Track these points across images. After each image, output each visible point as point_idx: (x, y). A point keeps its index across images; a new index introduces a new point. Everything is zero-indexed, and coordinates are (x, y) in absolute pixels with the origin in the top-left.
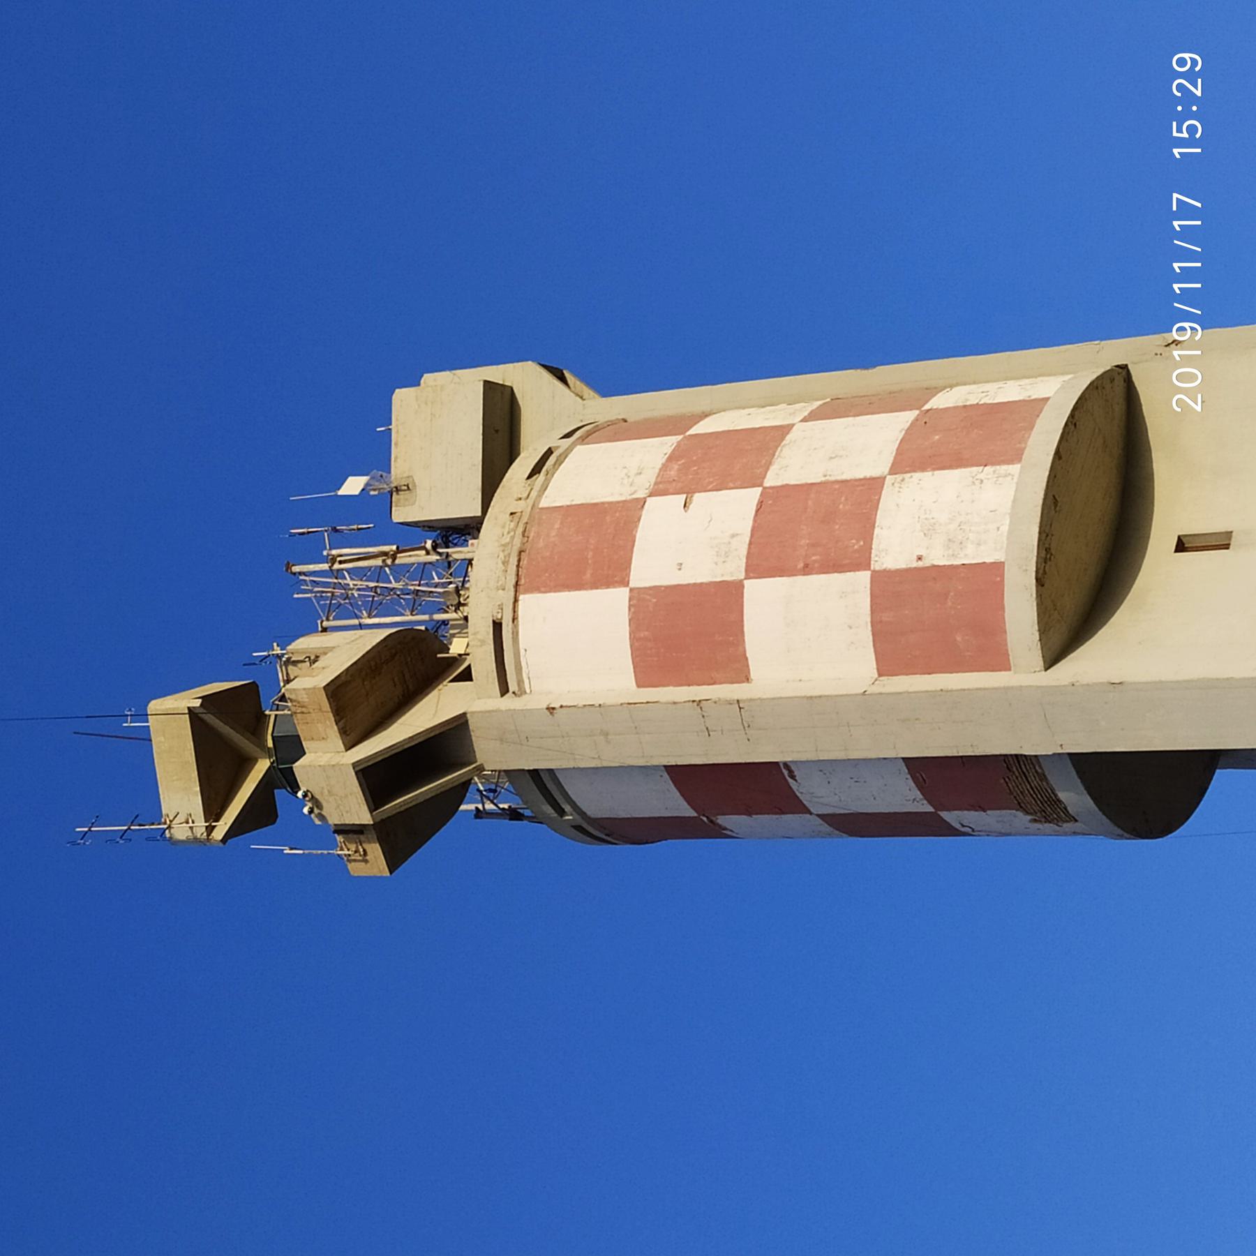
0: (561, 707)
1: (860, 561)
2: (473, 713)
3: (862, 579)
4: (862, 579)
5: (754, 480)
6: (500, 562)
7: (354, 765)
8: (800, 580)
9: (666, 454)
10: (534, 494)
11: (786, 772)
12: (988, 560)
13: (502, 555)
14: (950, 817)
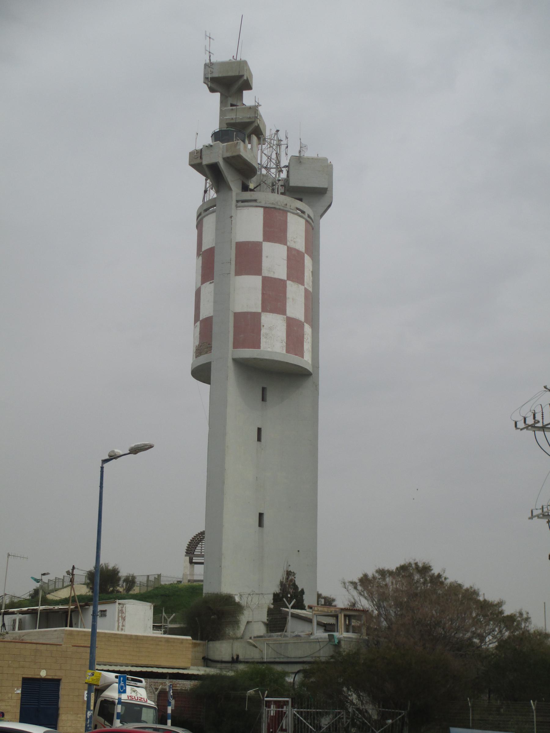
0: (232, 220)
1: (264, 309)
2: (232, 193)
3: (259, 310)
4: (259, 310)
5: (289, 278)
6: (273, 202)
7: (218, 162)
8: (260, 292)
9: (225, 494)
10: (291, 211)
11: (211, 281)
12: (261, 345)
13: (275, 202)
14: (198, 323)
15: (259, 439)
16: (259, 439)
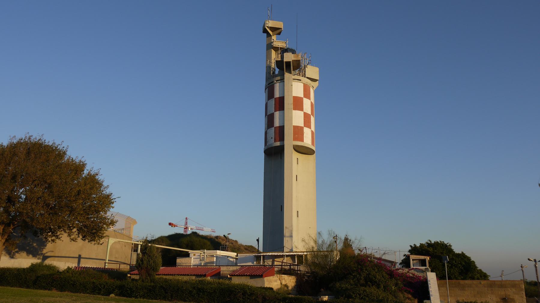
15: (297, 180)
16: (297, 180)
